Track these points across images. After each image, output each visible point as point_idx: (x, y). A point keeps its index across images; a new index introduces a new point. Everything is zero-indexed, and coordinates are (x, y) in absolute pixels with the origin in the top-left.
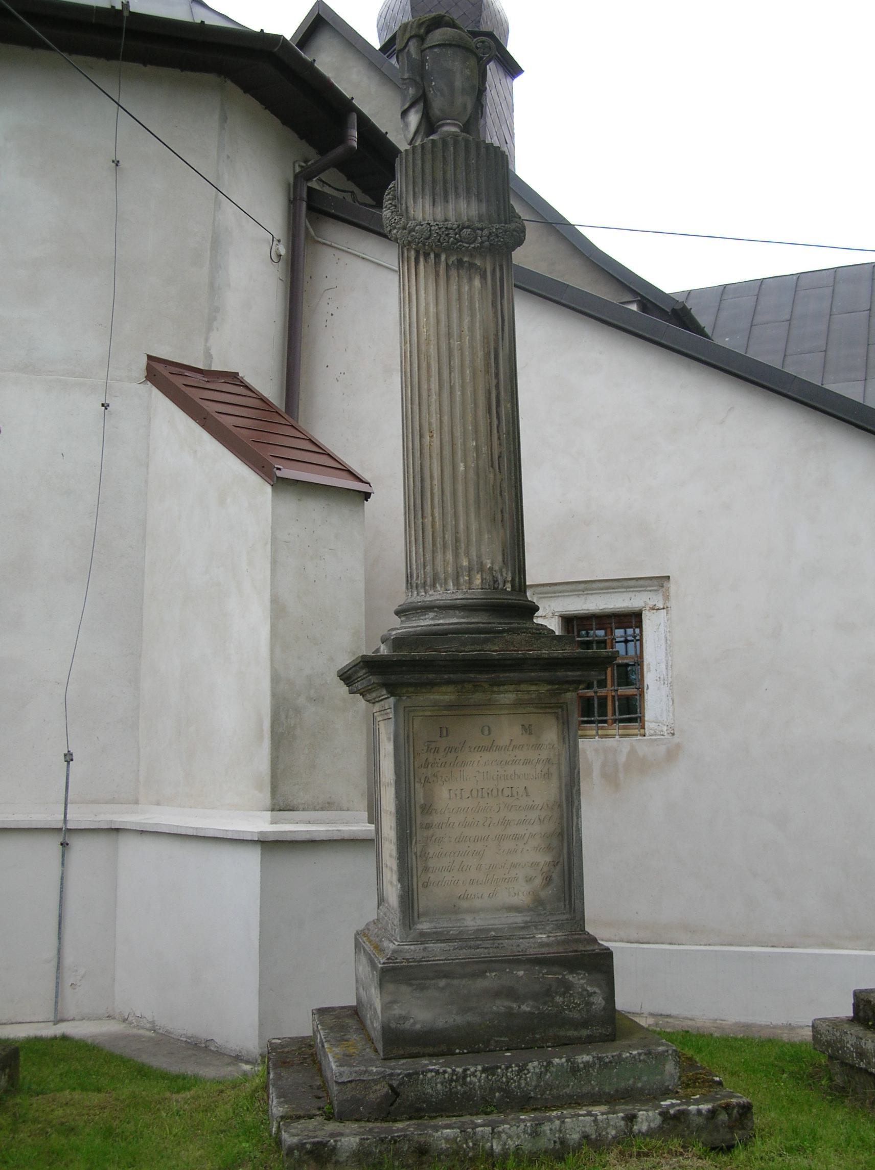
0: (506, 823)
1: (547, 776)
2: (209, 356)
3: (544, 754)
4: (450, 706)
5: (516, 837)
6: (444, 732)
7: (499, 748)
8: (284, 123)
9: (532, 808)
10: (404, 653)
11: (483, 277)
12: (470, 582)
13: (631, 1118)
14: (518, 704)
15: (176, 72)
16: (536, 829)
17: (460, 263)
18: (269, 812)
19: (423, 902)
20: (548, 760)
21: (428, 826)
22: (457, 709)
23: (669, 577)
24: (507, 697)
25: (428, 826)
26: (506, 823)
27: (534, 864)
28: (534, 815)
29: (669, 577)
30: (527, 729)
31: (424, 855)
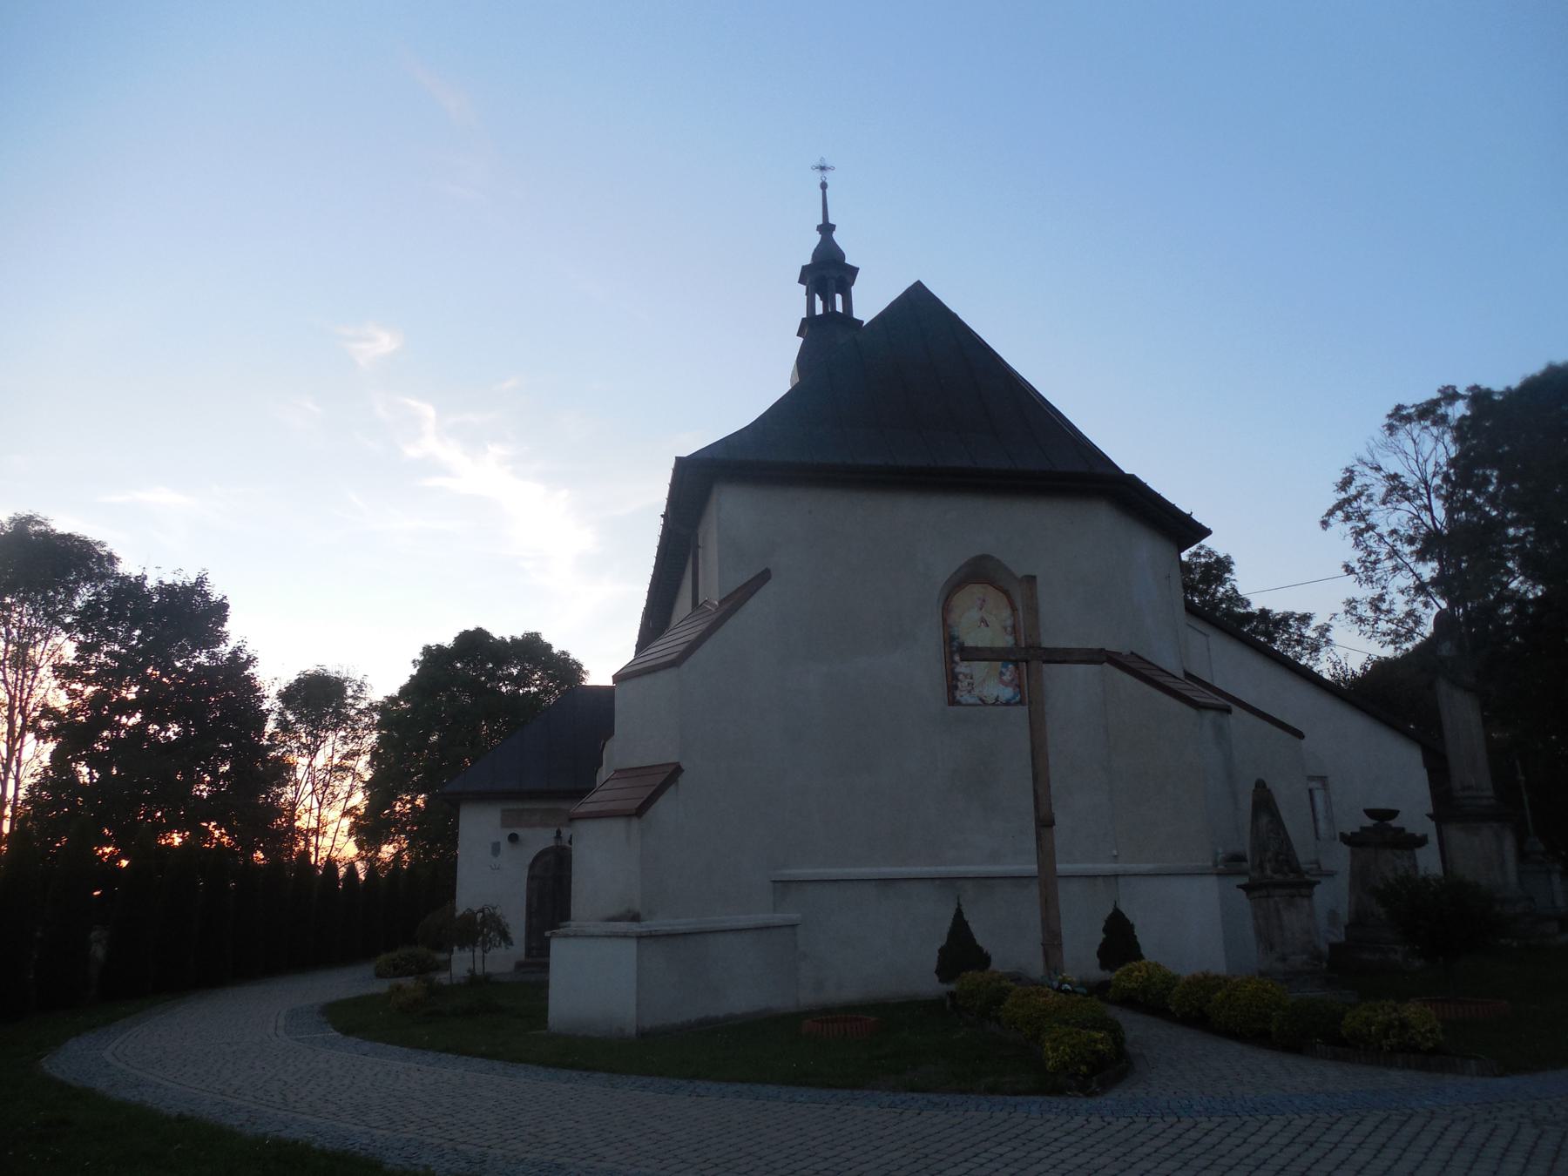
18: (1211, 883)
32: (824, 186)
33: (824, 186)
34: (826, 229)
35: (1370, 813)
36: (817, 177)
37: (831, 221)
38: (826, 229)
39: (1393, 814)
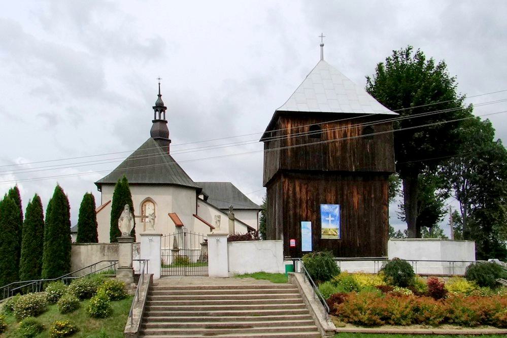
32: (159, 84)
33: (159, 84)
34: (160, 96)
36: (158, 82)
37: (161, 94)
38: (160, 96)
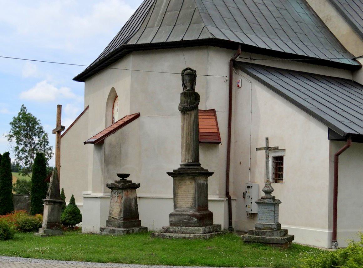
0: (187, 195)
1: (193, 189)
2: (206, 107)
3: (193, 186)
4: (180, 179)
5: (189, 198)
6: (180, 183)
7: (187, 185)
8: (227, 48)
9: (191, 193)
10: (174, 172)
11: (188, 114)
12: (186, 161)
13: (190, 235)
14: (189, 179)
15: (198, 47)
16: (192, 196)
17: (185, 113)
19: (178, 205)
20: (193, 187)
21: (178, 196)
22: (182, 180)
23: (285, 149)
24: (187, 178)
25: (178, 196)
26: (187, 195)
27: (191, 202)
28: (191, 194)
29: (285, 149)
30: (191, 183)
31: (177, 200)
35: (119, 175)
39: (128, 175)
